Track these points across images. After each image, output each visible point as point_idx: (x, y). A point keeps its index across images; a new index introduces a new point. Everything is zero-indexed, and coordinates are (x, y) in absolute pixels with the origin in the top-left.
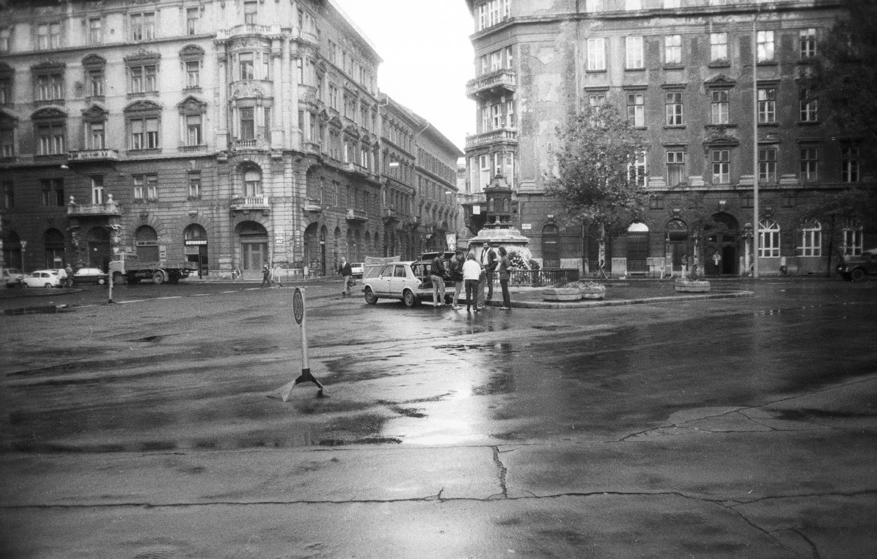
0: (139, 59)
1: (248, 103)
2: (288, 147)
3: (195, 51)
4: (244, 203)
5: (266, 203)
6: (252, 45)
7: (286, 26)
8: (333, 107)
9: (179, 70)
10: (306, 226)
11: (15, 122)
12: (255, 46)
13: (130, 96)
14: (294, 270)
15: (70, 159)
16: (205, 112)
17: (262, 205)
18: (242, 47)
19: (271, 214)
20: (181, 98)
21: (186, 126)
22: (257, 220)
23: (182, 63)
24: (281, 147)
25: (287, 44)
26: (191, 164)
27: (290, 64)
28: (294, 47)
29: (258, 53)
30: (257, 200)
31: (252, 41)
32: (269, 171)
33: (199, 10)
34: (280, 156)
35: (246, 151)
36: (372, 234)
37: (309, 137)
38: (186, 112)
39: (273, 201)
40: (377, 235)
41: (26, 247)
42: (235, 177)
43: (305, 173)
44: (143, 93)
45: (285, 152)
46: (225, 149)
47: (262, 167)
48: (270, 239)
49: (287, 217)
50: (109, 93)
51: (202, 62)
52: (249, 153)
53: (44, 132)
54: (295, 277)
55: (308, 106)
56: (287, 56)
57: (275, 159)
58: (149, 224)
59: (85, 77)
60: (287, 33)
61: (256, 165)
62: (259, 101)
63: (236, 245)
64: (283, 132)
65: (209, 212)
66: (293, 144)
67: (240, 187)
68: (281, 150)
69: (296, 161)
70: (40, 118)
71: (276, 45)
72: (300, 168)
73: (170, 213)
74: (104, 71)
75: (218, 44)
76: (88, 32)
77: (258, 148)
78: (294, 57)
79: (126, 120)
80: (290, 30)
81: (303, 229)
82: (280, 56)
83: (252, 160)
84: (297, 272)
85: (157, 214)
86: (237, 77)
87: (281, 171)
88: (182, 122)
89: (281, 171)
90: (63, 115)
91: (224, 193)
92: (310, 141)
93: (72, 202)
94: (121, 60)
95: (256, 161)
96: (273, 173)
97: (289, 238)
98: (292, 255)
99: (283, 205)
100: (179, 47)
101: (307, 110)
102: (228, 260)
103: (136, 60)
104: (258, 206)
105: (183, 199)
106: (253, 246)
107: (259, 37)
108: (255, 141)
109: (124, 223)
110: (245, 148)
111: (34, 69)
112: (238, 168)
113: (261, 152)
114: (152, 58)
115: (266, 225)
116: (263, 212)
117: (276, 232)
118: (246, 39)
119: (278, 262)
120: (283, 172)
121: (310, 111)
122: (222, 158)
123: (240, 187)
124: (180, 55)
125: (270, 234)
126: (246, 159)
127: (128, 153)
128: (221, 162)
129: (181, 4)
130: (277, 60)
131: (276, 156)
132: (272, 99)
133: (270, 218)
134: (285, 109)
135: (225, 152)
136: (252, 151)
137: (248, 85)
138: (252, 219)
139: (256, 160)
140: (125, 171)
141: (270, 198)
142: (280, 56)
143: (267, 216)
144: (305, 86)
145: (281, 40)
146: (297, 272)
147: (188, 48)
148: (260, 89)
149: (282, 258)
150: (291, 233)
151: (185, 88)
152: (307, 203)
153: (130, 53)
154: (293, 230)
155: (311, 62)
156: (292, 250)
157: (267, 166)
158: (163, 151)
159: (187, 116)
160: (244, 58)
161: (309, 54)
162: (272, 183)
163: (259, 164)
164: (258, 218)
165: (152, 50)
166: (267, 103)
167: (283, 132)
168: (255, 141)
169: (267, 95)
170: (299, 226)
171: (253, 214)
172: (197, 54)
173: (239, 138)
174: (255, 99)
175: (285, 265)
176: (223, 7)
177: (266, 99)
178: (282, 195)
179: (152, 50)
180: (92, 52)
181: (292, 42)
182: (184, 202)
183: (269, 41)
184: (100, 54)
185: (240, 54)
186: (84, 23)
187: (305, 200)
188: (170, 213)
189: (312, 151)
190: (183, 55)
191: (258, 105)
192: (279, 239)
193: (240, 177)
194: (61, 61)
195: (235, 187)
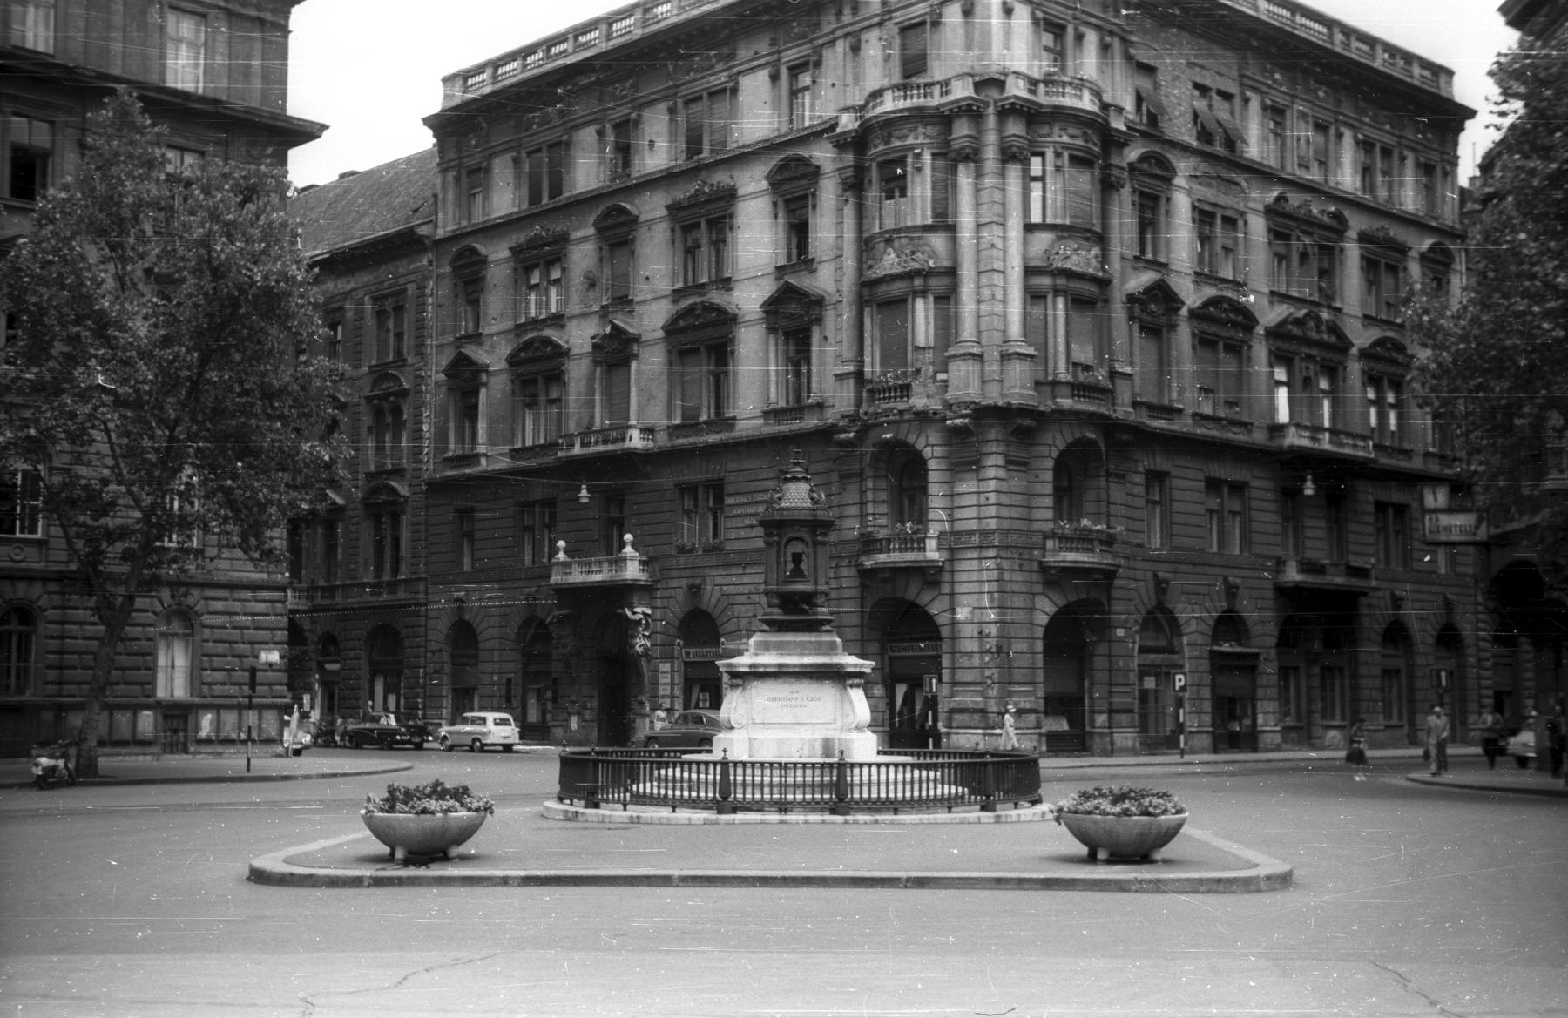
5: (932, 553)
6: (904, 137)
9: (768, 221)
12: (910, 141)
13: (677, 295)
19: (946, 577)
28: (1015, 128)
29: (918, 156)
33: (928, 26)
36: (1422, 630)
39: (954, 543)
40: (1448, 638)
43: (1050, 464)
44: (703, 285)
45: (984, 414)
48: (945, 647)
50: (641, 292)
51: (814, 194)
56: (990, 153)
58: (704, 607)
59: (601, 259)
67: (883, 509)
71: (962, 129)
73: (746, 580)
74: (633, 241)
75: (841, 144)
78: (1009, 155)
79: (669, 352)
82: (972, 156)
85: (719, 580)
88: (772, 348)
90: (561, 353)
93: (561, 556)
94: (663, 212)
95: (911, 439)
109: (659, 603)
111: (516, 251)
113: (923, 418)
115: (933, 610)
116: (930, 576)
118: (891, 124)
125: (945, 632)
127: (674, 431)
129: (775, 57)
140: (667, 479)
153: (682, 192)
155: (1074, 160)
162: (952, 495)
163: (920, 445)
164: (912, 592)
165: (721, 178)
166: (937, 284)
178: (973, 525)
179: (721, 178)
180: (790, 152)
184: (803, 152)
188: (746, 580)
190: (778, 182)
191: (915, 294)
195: (870, 508)
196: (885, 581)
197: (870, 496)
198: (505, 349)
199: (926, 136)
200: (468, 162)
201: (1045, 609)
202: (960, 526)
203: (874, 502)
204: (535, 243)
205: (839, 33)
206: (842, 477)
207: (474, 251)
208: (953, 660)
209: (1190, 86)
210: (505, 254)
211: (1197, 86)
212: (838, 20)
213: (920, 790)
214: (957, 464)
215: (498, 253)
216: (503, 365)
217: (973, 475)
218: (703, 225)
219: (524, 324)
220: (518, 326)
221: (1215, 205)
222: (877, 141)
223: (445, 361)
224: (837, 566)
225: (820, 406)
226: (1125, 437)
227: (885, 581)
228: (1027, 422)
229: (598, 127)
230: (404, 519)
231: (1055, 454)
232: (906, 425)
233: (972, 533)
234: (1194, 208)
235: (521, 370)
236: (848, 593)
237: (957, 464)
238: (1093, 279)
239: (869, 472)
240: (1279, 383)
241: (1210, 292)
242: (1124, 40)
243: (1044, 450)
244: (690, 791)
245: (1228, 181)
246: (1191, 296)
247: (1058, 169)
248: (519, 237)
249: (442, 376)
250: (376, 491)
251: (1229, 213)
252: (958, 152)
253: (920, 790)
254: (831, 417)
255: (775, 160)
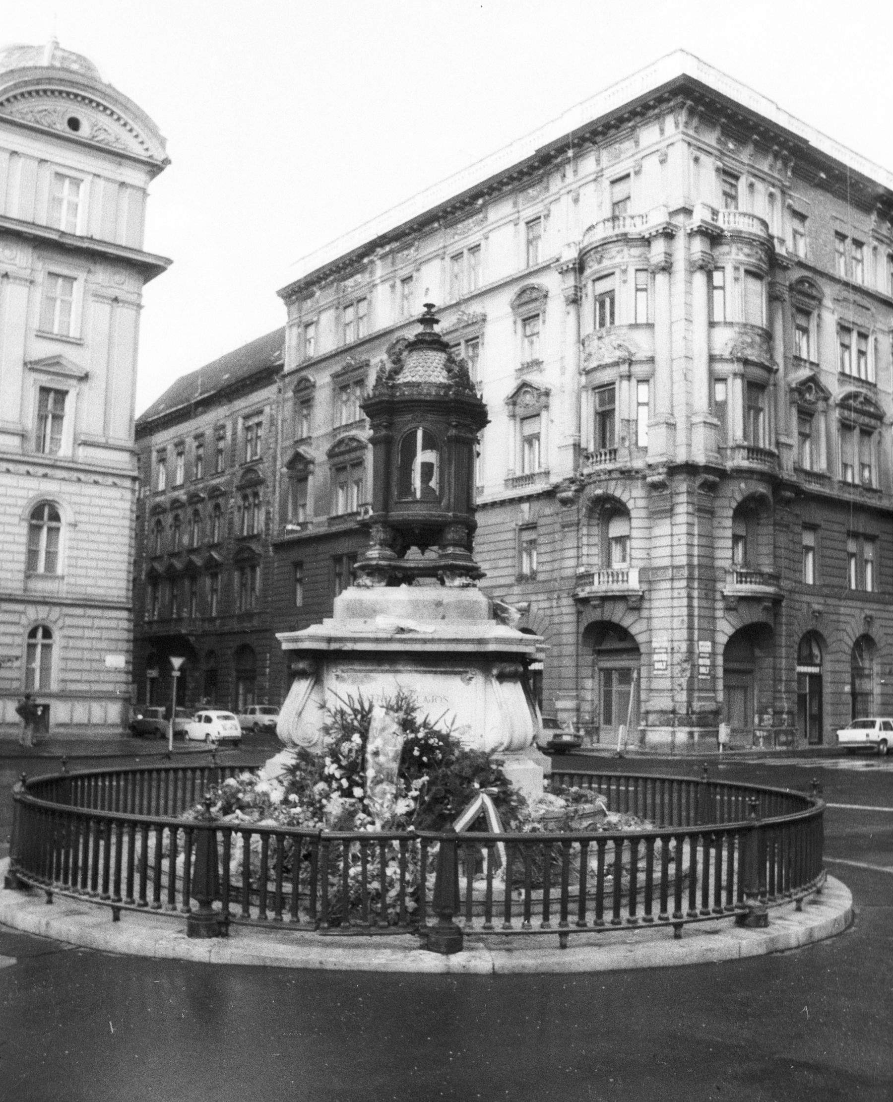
0: (456, 330)
1: (605, 376)
2: (681, 458)
3: (535, 294)
4: (592, 583)
5: (633, 583)
6: (613, 258)
7: (679, 204)
8: (847, 371)
10: (730, 631)
11: (311, 467)
12: (618, 260)
14: (687, 729)
15: (359, 518)
16: (547, 407)
17: (624, 586)
18: (596, 267)
20: (510, 387)
21: (519, 438)
22: (616, 619)
23: (515, 323)
24: (664, 459)
25: (681, 240)
26: (522, 512)
27: (689, 282)
28: (698, 245)
29: (625, 271)
30: (616, 576)
31: (613, 249)
32: (643, 513)
34: (661, 477)
35: (597, 473)
37: (739, 433)
38: (520, 411)
39: (648, 575)
41: (181, 669)
42: (585, 531)
43: (730, 513)
45: (674, 470)
46: (571, 474)
47: (630, 505)
49: (676, 612)
51: (544, 312)
52: (603, 477)
53: (342, 478)
54: (690, 746)
55: (738, 367)
56: (680, 266)
57: (655, 486)
60: (680, 220)
61: (618, 501)
62: (624, 368)
63: (587, 672)
64: (671, 426)
65: (546, 605)
66: (694, 449)
68: (664, 465)
69: (702, 486)
70: (337, 455)
72: (718, 503)
76: (398, 300)
77: (618, 465)
80: (687, 211)
81: (722, 639)
82: (667, 268)
83: (610, 492)
84: (696, 735)
86: (588, 327)
87: (665, 511)
89: (665, 511)
91: (569, 566)
92: (739, 442)
95: (618, 493)
96: (654, 515)
97: (678, 657)
98: (682, 697)
99: (667, 585)
100: (509, 294)
101: (735, 374)
102: (570, 704)
103: (452, 332)
104: (616, 588)
105: (509, 580)
106: (620, 675)
107: (625, 239)
108: (615, 451)
110: (598, 467)
111: (335, 376)
112: (591, 512)
113: (627, 474)
114: (473, 324)
115: (633, 630)
117: (654, 645)
119: (655, 712)
120: (670, 512)
121: (743, 376)
122: (564, 495)
123: (595, 550)
124: (513, 308)
125: (643, 649)
126: (599, 492)
128: (565, 502)
130: (661, 278)
131: (656, 478)
132: (652, 360)
133: (645, 613)
134: (678, 377)
135: (572, 481)
136: (610, 472)
137: (606, 340)
138: (606, 617)
139: (618, 491)
141: (643, 571)
142: (667, 268)
143: (638, 609)
144: (731, 324)
145: (668, 235)
146: (696, 735)
147: (523, 292)
148: (627, 344)
149: (662, 702)
150: (684, 647)
151: (519, 366)
152: (731, 579)
154: (690, 640)
155: (747, 272)
156: (685, 685)
157: (642, 503)
158: (485, 491)
159: (523, 419)
160: (603, 286)
161: (742, 257)
163: (624, 498)
164: (618, 614)
167: (671, 426)
168: (615, 451)
169: (640, 355)
170: (710, 634)
171: (608, 606)
172: (536, 299)
173: (591, 449)
174: (616, 364)
175: (670, 717)
176: (576, 200)
177: (641, 362)
178: (666, 562)
179: (475, 308)
181: (691, 235)
182: (510, 586)
183: (646, 242)
185: (594, 281)
186: (393, 287)
187: (726, 572)
189: (745, 464)
192: (660, 660)
193: (595, 530)
194: (364, 357)
196: (595, 607)
197: (585, 540)
198: (326, 446)
199: (630, 256)
200: (306, 319)
201: (725, 628)
202: (657, 563)
203: (588, 545)
204: (346, 371)
205: (562, 192)
206: (563, 527)
207: (307, 380)
208: (649, 672)
209: (833, 233)
210: (328, 379)
211: (838, 234)
212: (563, 181)
213: (145, 847)
214: (654, 513)
215: (323, 379)
216: (324, 458)
217: (668, 521)
218: (632, 175)
219: (339, 428)
220: (334, 430)
221: (854, 323)
222: (591, 264)
223: (287, 458)
224: (559, 598)
225: (547, 474)
226: (788, 494)
227: (595, 607)
228: (711, 478)
229: (391, 282)
230: (258, 570)
231: (734, 505)
232: (614, 482)
233: (665, 568)
234: (839, 324)
235: (336, 460)
236: (565, 610)
237: (654, 513)
238: (761, 366)
239: (584, 521)
240: (808, 549)
241: (851, 388)
242: (783, 193)
243: (725, 502)
244: (627, 791)
245: (863, 307)
246: (837, 391)
247: (736, 279)
248: (337, 368)
249: (285, 470)
250: (241, 550)
251: (863, 330)
252: (657, 266)
253: (145, 847)
254: (554, 479)
255: (516, 289)
